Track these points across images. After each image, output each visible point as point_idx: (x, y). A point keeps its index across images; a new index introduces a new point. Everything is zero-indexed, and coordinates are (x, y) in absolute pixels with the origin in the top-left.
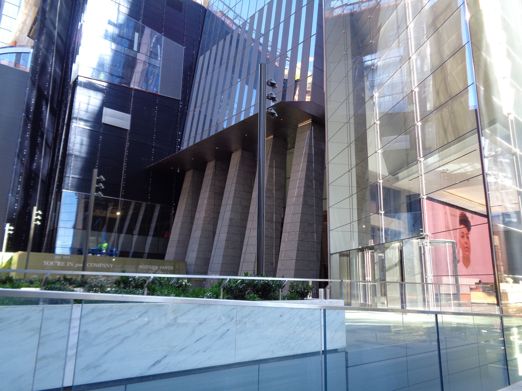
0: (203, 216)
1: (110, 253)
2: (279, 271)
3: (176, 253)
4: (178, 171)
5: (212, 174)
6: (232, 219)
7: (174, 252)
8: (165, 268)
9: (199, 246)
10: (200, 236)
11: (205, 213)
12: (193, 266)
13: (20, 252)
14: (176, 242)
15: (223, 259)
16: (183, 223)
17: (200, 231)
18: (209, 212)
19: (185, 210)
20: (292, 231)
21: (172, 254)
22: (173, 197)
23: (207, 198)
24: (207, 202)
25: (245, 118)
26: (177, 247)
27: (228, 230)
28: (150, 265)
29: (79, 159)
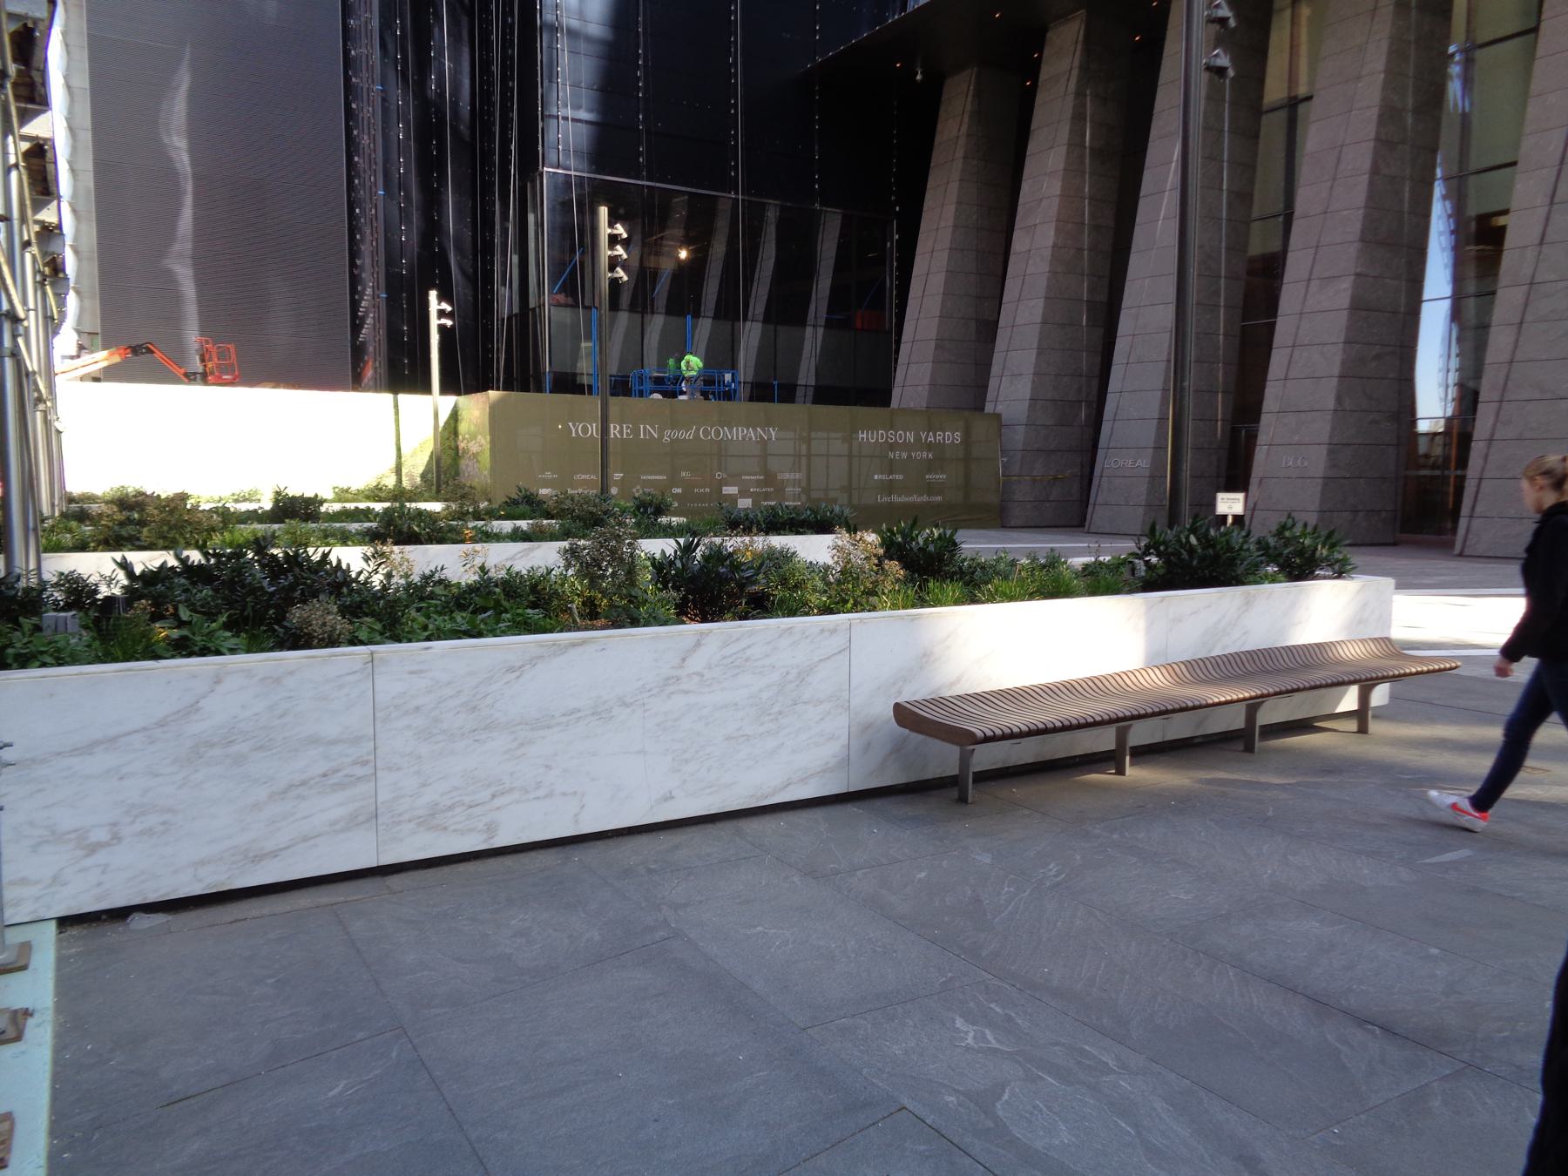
0: (1051, 243)
1: (710, 387)
2: (1481, 444)
3: (932, 385)
4: (919, 77)
5: (1075, 72)
7: (927, 381)
9: (1038, 354)
10: (1039, 320)
11: (1057, 230)
12: (1021, 429)
13: (493, 394)
14: (933, 344)
19: (955, 226)
20: (1553, 277)
21: (920, 388)
23: (1061, 173)
28: (891, 428)
29: (583, 46)
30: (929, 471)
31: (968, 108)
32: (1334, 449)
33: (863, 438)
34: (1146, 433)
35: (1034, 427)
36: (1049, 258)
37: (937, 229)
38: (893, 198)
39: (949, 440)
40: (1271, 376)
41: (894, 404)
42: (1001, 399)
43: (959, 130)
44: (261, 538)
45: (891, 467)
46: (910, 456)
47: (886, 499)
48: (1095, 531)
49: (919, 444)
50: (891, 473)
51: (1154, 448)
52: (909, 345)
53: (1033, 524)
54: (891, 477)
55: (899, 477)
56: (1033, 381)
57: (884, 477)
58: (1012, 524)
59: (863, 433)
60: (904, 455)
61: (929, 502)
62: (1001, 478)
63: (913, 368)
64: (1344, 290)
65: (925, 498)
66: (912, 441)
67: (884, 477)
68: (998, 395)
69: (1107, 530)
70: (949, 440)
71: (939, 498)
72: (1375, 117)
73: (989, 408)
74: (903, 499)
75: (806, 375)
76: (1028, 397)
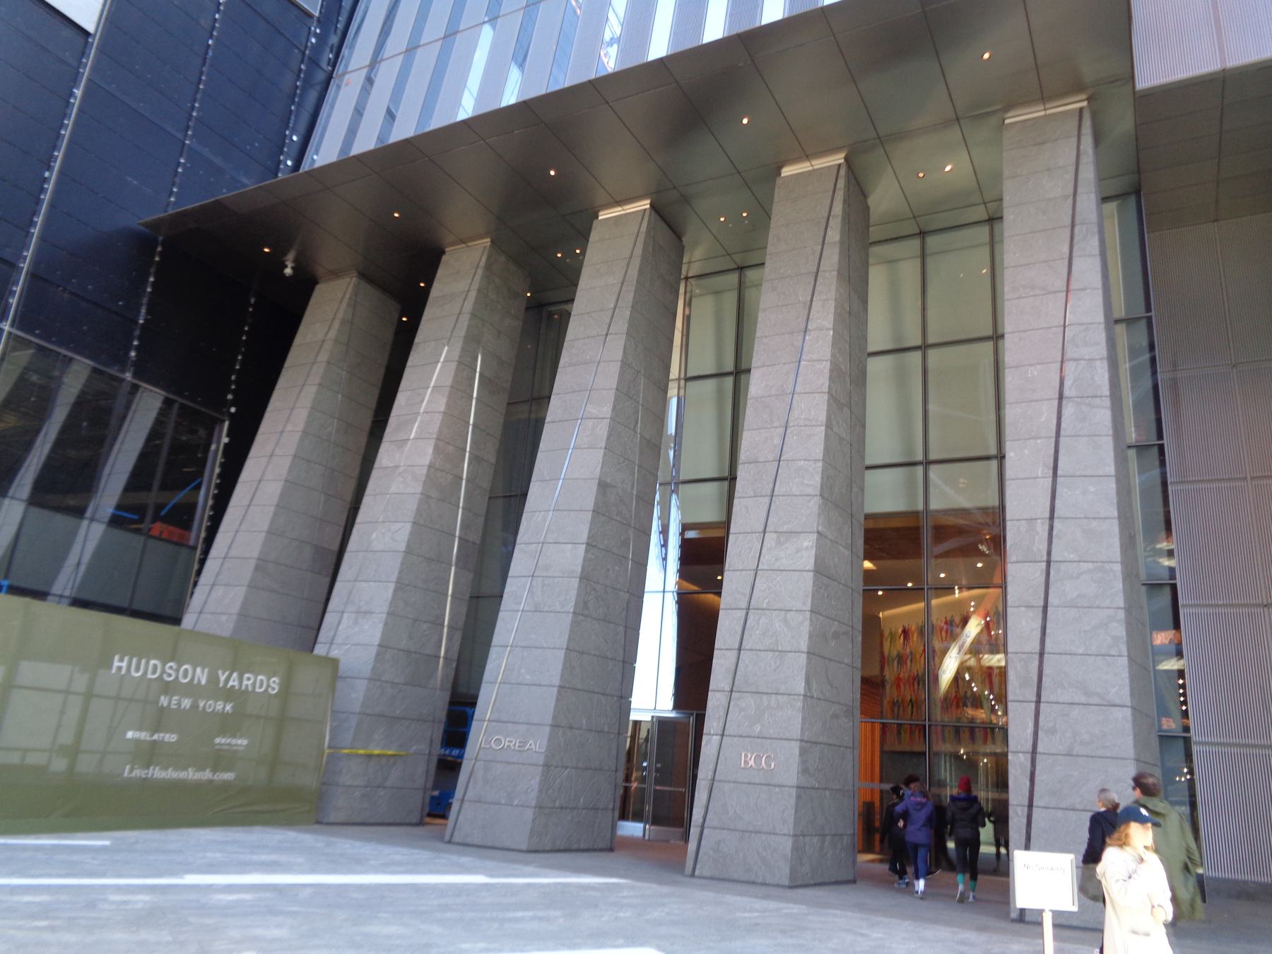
4: (288, 271)
5: (473, 294)
6: (610, 486)
7: (235, 608)
8: (245, 682)
9: (396, 591)
14: (252, 563)
15: (568, 666)
16: (290, 485)
17: (408, 528)
18: (451, 448)
19: (305, 433)
21: (224, 618)
22: (233, 377)
24: (448, 405)
25: (795, 13)
26: (252, 586)
27: (590, 530)
30: (223, 732)
31: (340, 315)
32: (807, 745)
33: (120, 668)
34: (542, 705)
35: (378, 683)
36: (424, 478)
37: (282, 432)
38: (244, 338)
39: (261, 686)
40: (718, 643)
41: (188, 620)
42: (339, 640)
43: (326, 334)
44: (996, 671)
45: (160, 720)
46: (194, 706)
47: (138, 773)
48: (460, 841)
49: (215, 690)
50: (156, 730)
51: (551, 725)
52: (218, 562)
53: (358, 820)
54: (155, 737)
55: (171, 738)
56: (386, 624)
57: (143, 735)
58: (332, 819)
59: (121, 660)
60: (187, 703)
61: (211, 781)
62: (327, 751)
63: (219, 592)
64: (807, 548)
65: (207, 775)
66: (203, 682)
67: (143, 735)
68: (335, 635)
69: (476, 841)
70: (261, 686)
71: (229, 776)
72: (827, 371)
73: (320, 650)
74: (171, 774)
75: (65, 582)
76: (377, 643)
